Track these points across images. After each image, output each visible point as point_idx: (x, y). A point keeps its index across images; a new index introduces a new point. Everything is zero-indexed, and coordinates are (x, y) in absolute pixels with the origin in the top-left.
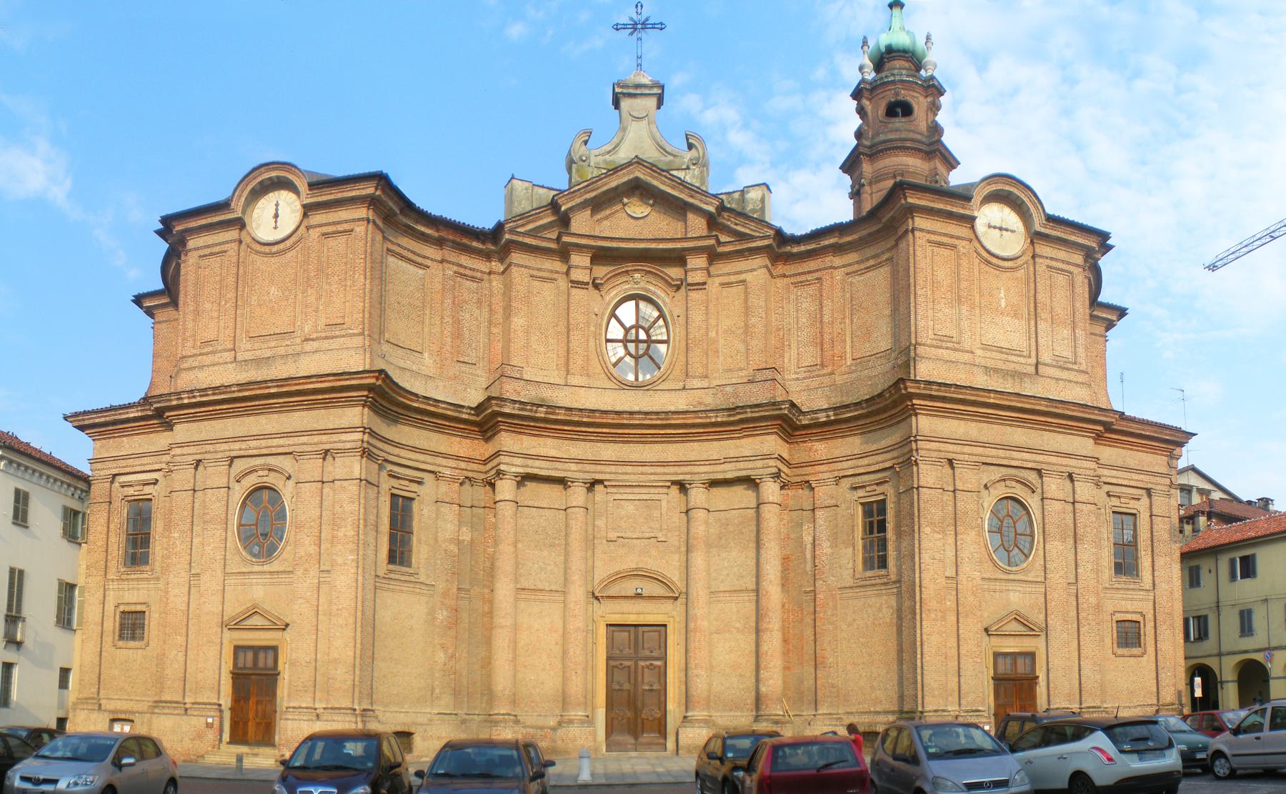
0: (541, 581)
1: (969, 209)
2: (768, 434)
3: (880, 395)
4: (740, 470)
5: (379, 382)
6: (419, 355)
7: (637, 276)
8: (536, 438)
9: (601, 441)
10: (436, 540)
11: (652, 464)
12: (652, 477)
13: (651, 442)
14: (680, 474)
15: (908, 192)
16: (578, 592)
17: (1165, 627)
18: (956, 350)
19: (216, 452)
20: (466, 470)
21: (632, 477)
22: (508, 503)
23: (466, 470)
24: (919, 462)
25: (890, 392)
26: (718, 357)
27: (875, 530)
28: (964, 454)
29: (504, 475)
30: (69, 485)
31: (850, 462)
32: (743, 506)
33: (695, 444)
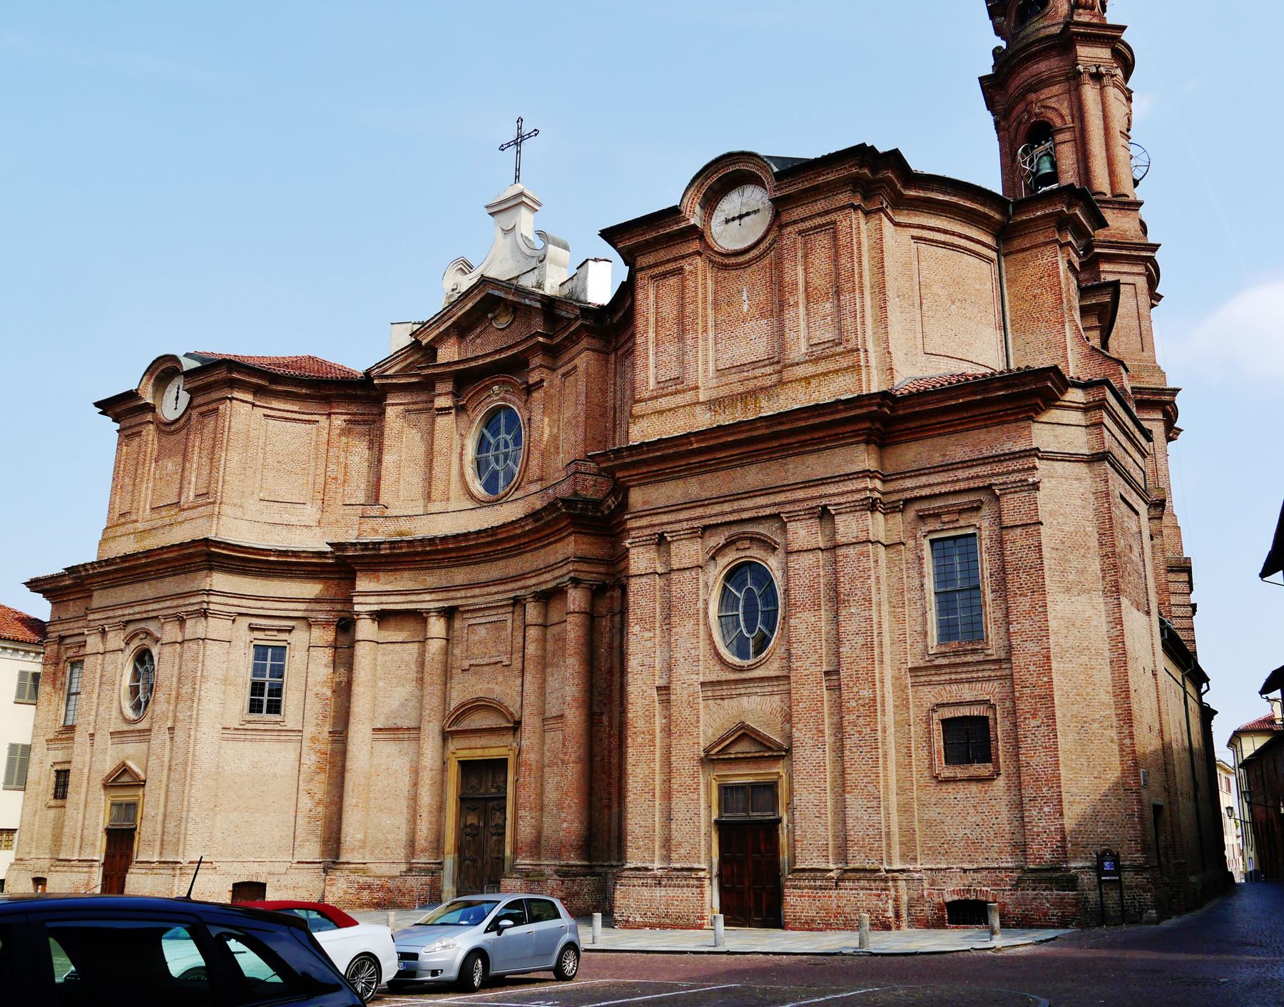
1: (684, 221)
6: (302, 506)
7: (496, 388)
12: (497, 597)
16: (431, 731)
17: (1034, 723)
18: (677, 392)
19: (114, 617)
21: (481, 600)
23: (343, 611)
26: (558, 453)
28: (680, 521)
29: (358, 615)
30: (517, 602)
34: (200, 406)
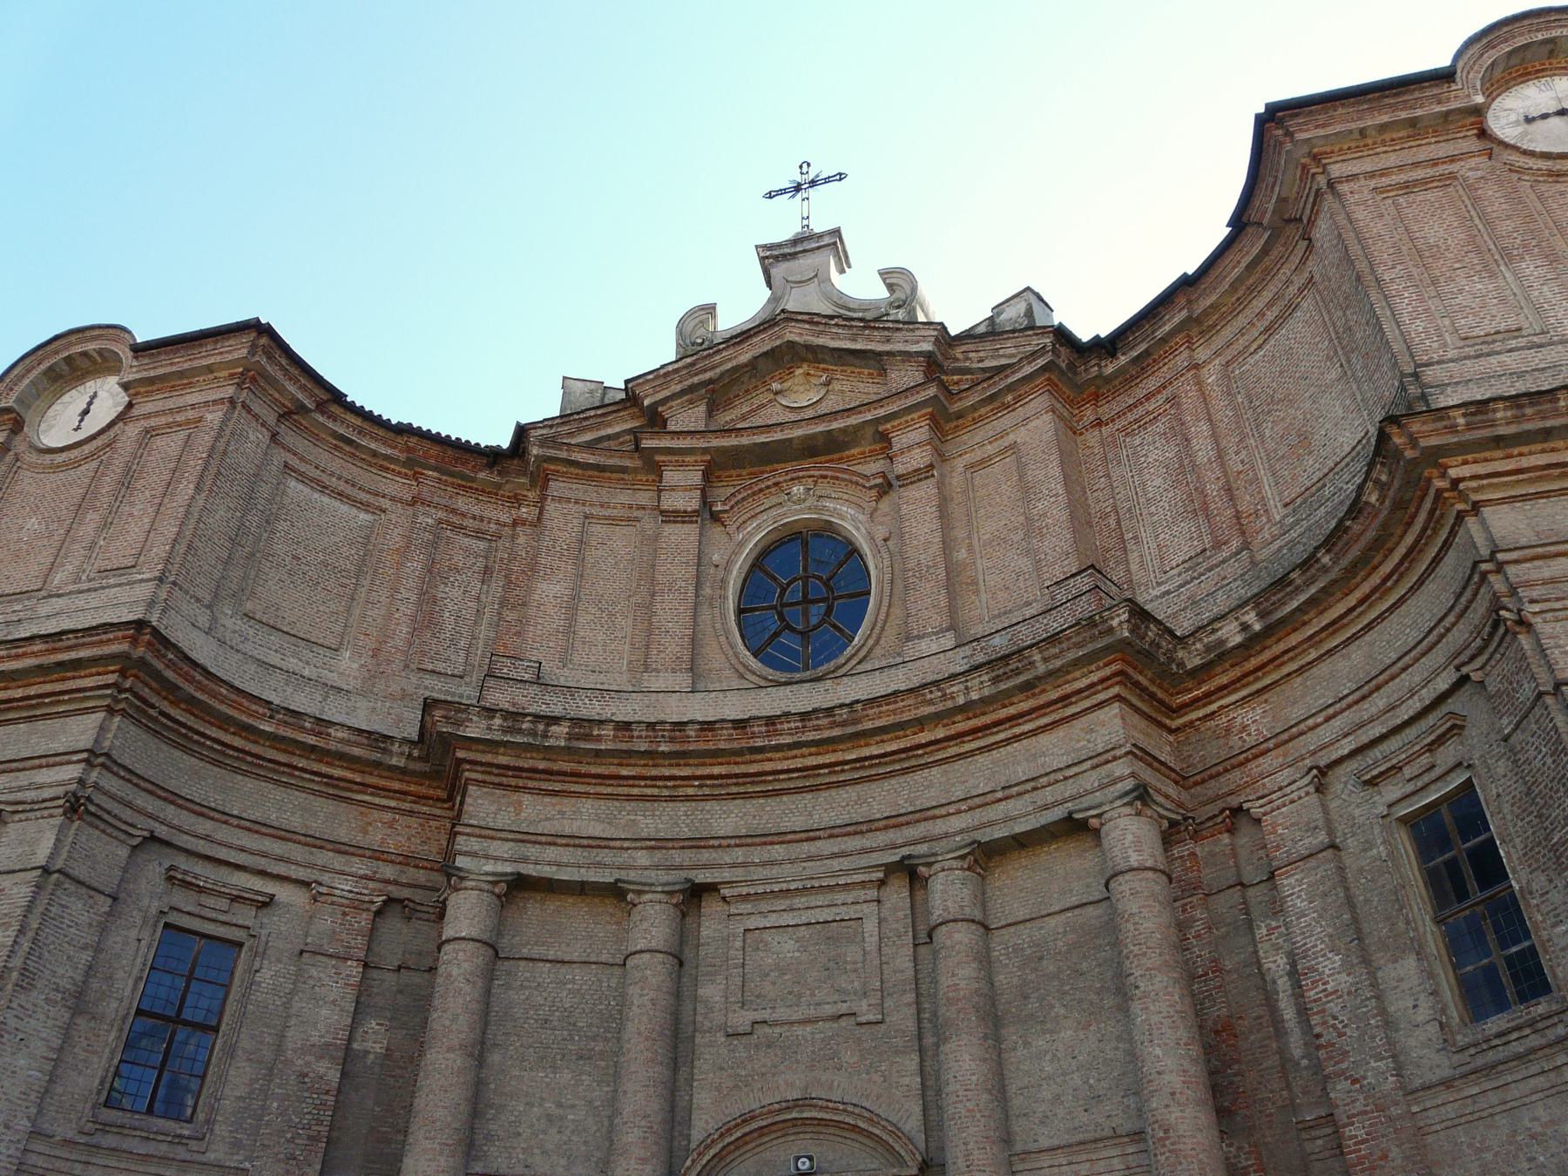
0: (545, 1153)
2: (1100, 705)
3: (1356, 508)
4: (1046, 807)
5: (140, 651)
8: (555, 800)
9: (714, 797)
10: (279, 1048)
11: (833, 832)
12: (836, 864)
13: (829, 786)
14: (886, 847)
15: (1292, 124)
20: (396, 883)
22: (463, 945)
23: (396, 883)
24: (1536, 620)
25: (1377, 482)
27: (1472, 885)
29: (462, 879)
31: (1336, 723)
32: (1074, 901)
33: (935, 770)
34: (147, 416)
